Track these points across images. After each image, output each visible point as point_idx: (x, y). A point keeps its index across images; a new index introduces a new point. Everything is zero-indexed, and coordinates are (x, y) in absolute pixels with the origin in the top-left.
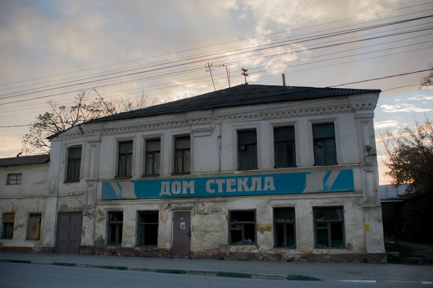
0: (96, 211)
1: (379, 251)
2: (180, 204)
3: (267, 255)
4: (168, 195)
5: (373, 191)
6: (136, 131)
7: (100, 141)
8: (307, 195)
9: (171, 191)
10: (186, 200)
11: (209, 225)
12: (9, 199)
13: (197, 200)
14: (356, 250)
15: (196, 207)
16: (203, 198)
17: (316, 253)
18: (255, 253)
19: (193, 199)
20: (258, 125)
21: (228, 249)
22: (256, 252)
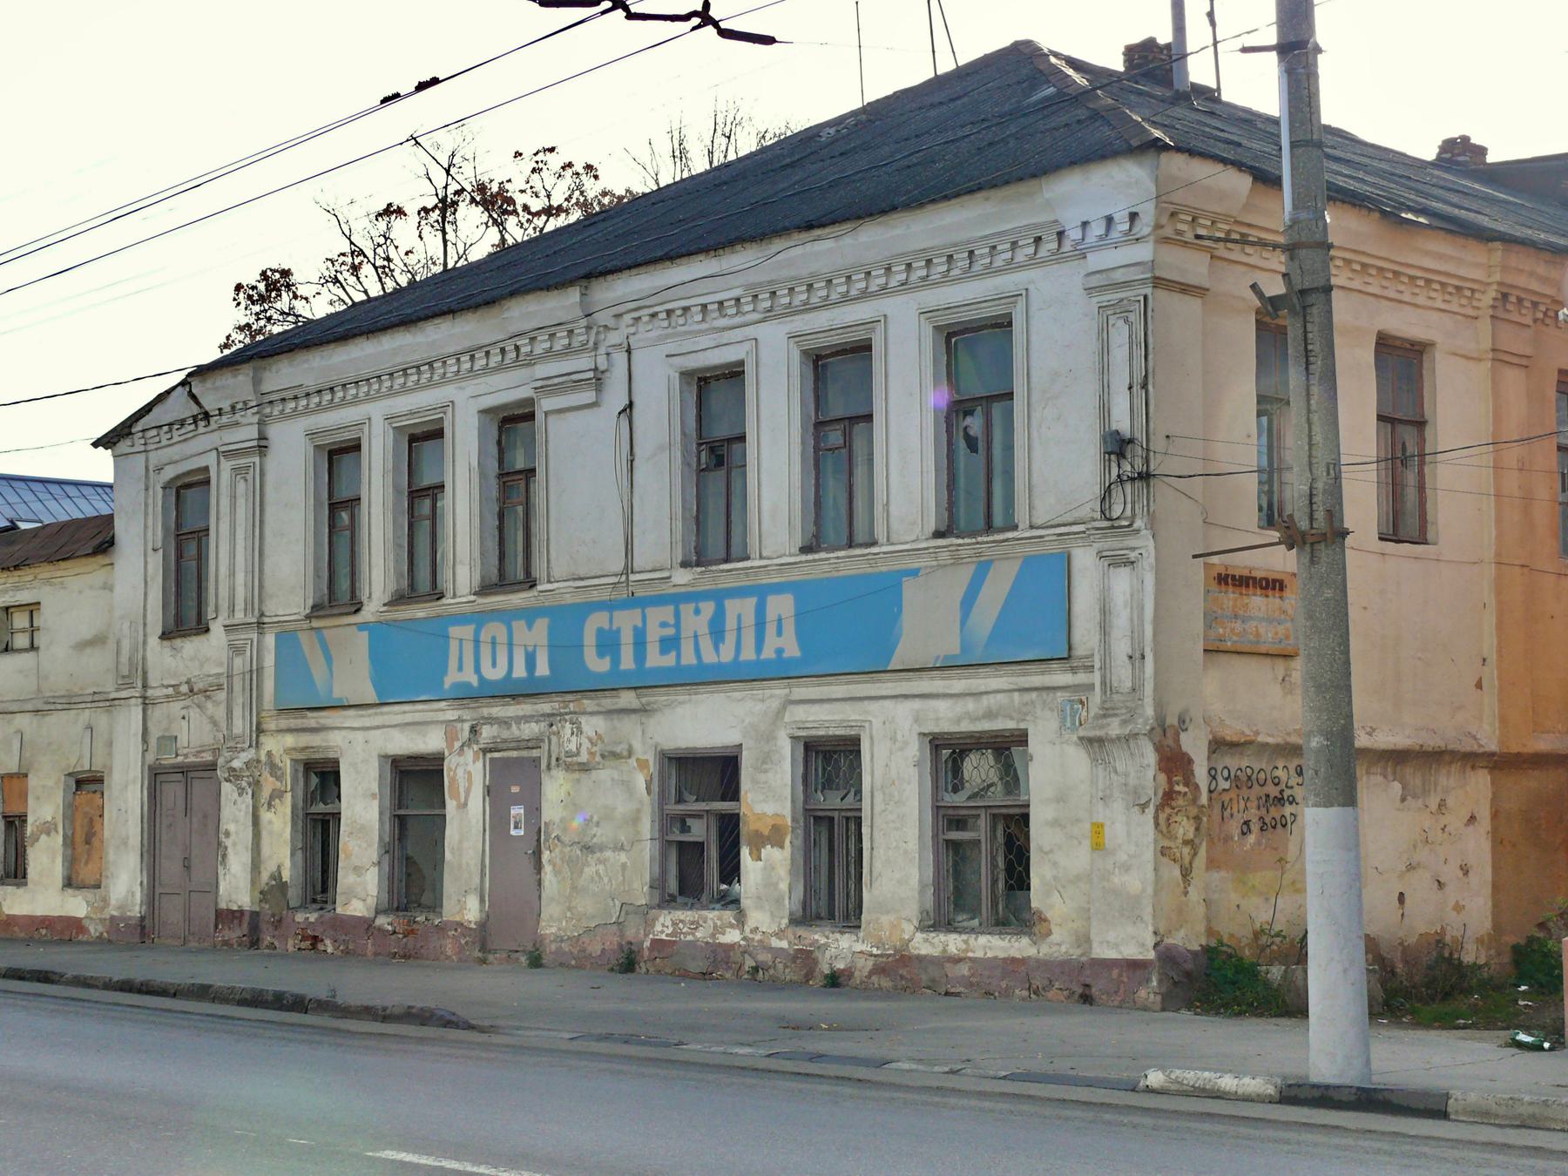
0: (258, 761)
1: (1131, 952)
2: (506, 723)
3: (770, 956)
4: (468, 685)
5: (1131, 657)
6: (369, 398)
7: (260, 447)
8: (909, 680)
9: (477, 670)
10: (526, 708)
11: (595, 819)
12: (9, 716)
13: (562, 705)
14: (1058, 944)
15: (554, 739)
16: (579, 696)
17: (925, 950)
18: (731, 947)
19: (548, 700)
20: (747, 346)
21: (649, 924)
22: (736, 940)
